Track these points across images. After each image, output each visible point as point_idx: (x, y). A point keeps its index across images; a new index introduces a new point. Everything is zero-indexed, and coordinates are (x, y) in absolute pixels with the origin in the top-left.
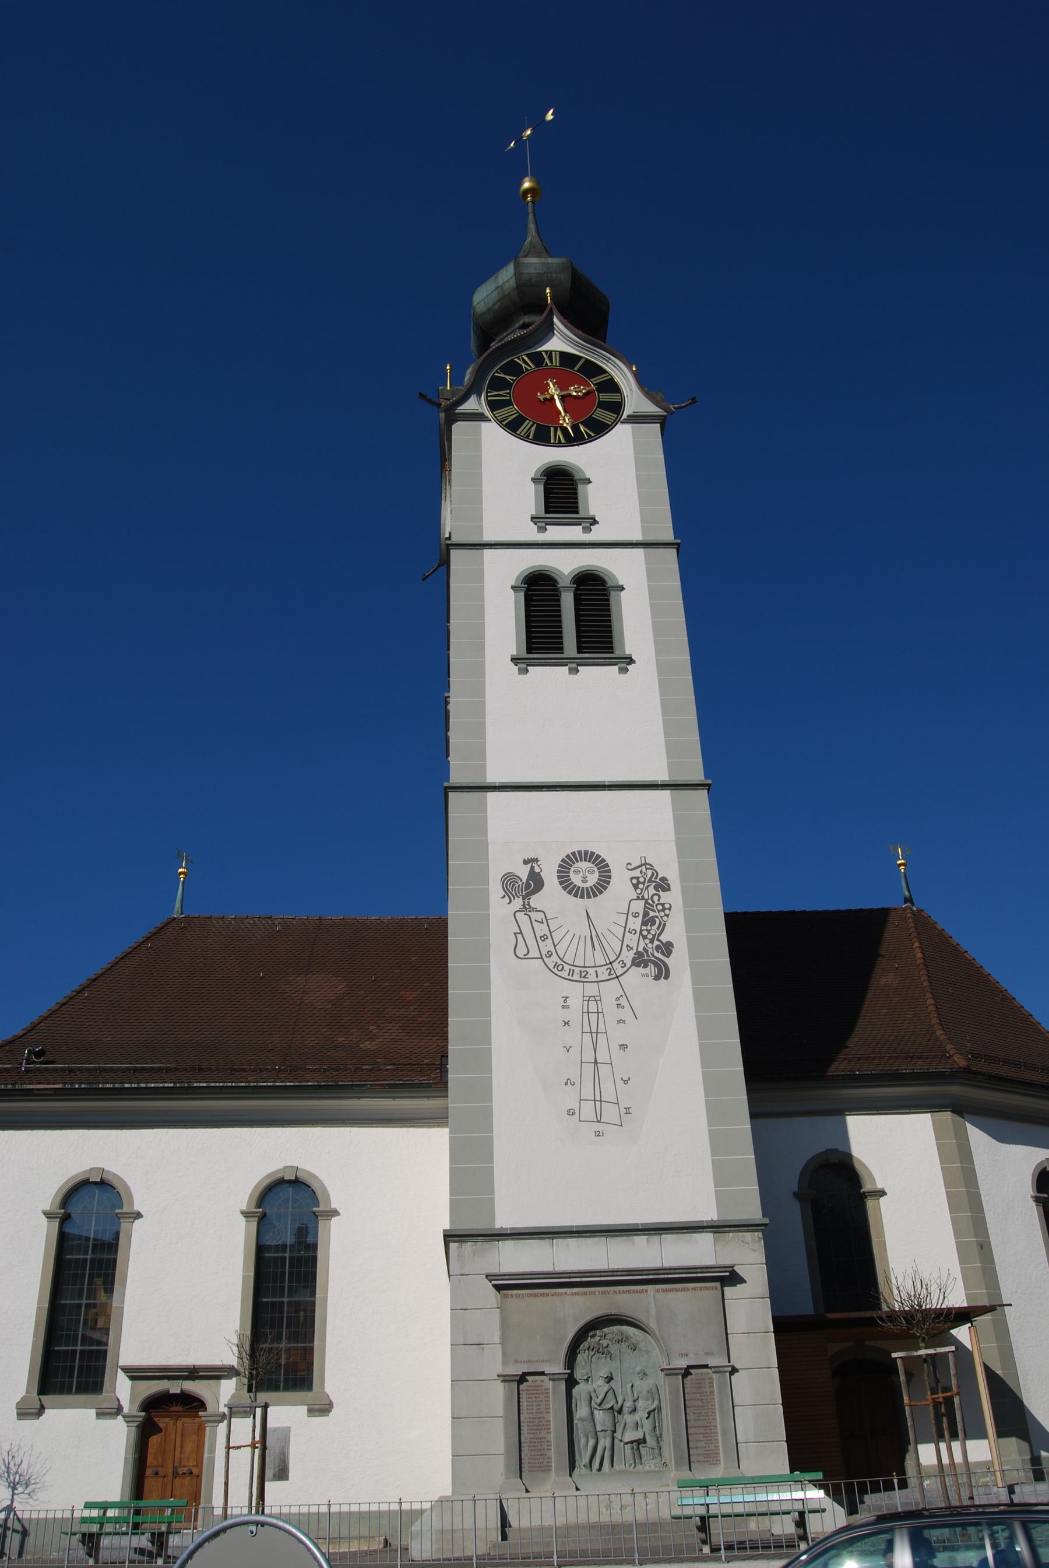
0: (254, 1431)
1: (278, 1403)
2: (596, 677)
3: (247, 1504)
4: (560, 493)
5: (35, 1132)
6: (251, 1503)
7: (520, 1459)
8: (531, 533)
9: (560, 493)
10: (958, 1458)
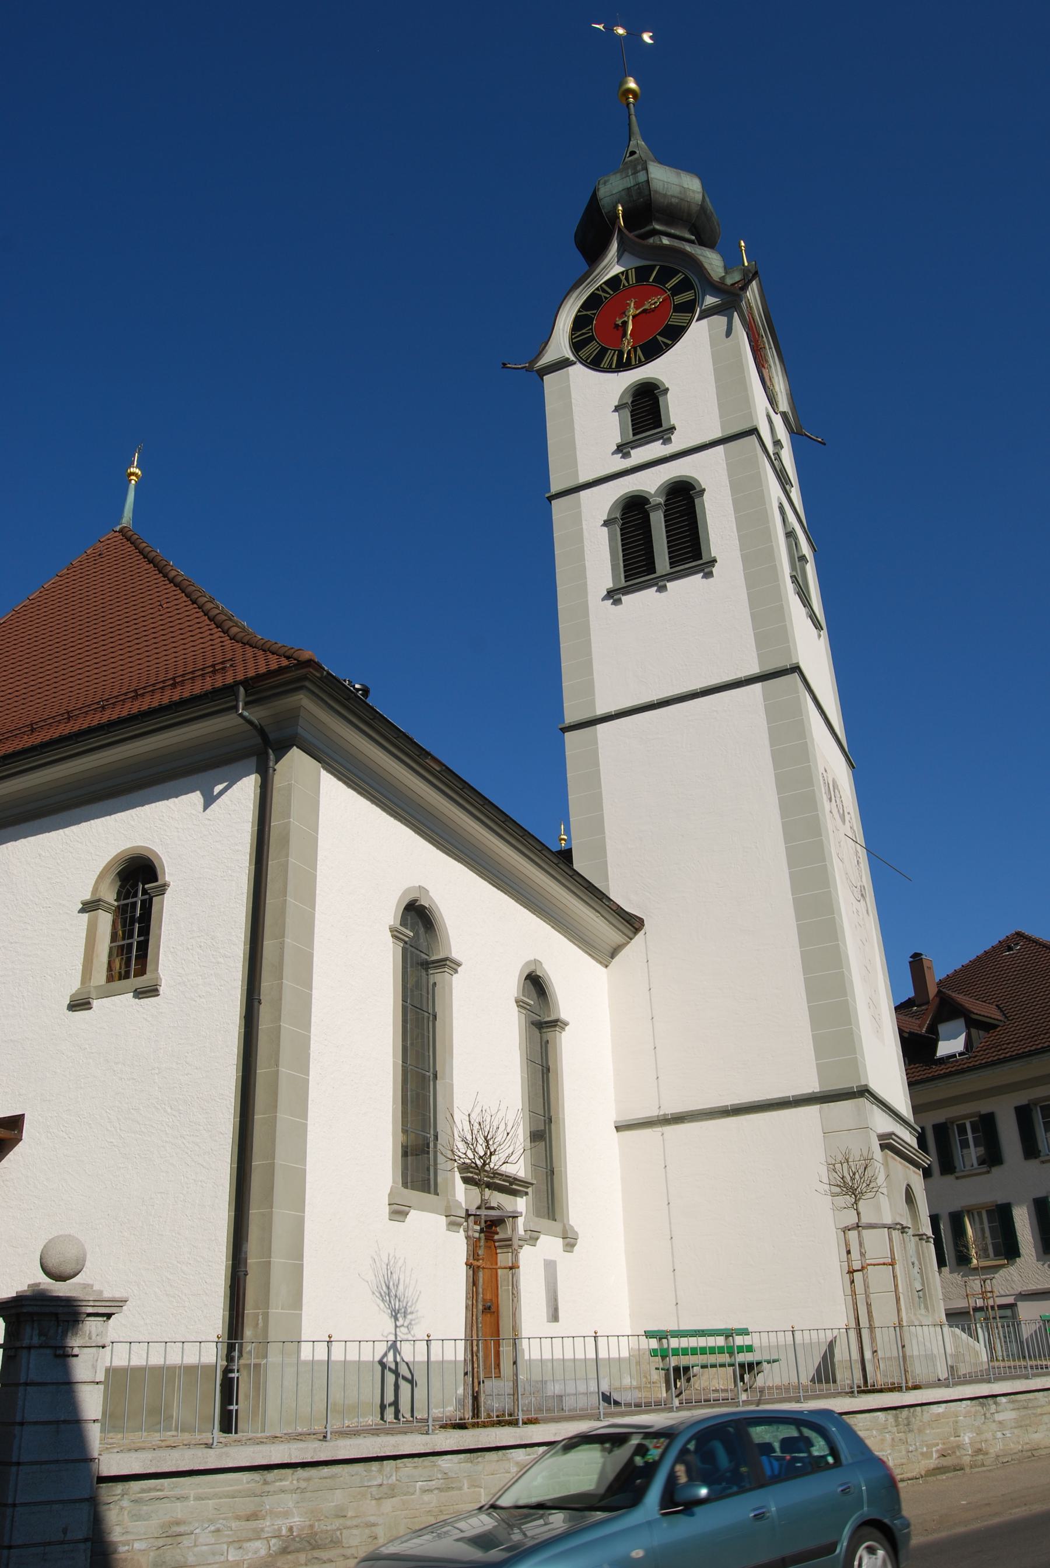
0: (869, 1305)
2: (687, 588)
3: (683, 1327)
4: (646, 412)
5: (374, 806)
8: (620, 463)
9: (646, 412)
10: (666, 1346)
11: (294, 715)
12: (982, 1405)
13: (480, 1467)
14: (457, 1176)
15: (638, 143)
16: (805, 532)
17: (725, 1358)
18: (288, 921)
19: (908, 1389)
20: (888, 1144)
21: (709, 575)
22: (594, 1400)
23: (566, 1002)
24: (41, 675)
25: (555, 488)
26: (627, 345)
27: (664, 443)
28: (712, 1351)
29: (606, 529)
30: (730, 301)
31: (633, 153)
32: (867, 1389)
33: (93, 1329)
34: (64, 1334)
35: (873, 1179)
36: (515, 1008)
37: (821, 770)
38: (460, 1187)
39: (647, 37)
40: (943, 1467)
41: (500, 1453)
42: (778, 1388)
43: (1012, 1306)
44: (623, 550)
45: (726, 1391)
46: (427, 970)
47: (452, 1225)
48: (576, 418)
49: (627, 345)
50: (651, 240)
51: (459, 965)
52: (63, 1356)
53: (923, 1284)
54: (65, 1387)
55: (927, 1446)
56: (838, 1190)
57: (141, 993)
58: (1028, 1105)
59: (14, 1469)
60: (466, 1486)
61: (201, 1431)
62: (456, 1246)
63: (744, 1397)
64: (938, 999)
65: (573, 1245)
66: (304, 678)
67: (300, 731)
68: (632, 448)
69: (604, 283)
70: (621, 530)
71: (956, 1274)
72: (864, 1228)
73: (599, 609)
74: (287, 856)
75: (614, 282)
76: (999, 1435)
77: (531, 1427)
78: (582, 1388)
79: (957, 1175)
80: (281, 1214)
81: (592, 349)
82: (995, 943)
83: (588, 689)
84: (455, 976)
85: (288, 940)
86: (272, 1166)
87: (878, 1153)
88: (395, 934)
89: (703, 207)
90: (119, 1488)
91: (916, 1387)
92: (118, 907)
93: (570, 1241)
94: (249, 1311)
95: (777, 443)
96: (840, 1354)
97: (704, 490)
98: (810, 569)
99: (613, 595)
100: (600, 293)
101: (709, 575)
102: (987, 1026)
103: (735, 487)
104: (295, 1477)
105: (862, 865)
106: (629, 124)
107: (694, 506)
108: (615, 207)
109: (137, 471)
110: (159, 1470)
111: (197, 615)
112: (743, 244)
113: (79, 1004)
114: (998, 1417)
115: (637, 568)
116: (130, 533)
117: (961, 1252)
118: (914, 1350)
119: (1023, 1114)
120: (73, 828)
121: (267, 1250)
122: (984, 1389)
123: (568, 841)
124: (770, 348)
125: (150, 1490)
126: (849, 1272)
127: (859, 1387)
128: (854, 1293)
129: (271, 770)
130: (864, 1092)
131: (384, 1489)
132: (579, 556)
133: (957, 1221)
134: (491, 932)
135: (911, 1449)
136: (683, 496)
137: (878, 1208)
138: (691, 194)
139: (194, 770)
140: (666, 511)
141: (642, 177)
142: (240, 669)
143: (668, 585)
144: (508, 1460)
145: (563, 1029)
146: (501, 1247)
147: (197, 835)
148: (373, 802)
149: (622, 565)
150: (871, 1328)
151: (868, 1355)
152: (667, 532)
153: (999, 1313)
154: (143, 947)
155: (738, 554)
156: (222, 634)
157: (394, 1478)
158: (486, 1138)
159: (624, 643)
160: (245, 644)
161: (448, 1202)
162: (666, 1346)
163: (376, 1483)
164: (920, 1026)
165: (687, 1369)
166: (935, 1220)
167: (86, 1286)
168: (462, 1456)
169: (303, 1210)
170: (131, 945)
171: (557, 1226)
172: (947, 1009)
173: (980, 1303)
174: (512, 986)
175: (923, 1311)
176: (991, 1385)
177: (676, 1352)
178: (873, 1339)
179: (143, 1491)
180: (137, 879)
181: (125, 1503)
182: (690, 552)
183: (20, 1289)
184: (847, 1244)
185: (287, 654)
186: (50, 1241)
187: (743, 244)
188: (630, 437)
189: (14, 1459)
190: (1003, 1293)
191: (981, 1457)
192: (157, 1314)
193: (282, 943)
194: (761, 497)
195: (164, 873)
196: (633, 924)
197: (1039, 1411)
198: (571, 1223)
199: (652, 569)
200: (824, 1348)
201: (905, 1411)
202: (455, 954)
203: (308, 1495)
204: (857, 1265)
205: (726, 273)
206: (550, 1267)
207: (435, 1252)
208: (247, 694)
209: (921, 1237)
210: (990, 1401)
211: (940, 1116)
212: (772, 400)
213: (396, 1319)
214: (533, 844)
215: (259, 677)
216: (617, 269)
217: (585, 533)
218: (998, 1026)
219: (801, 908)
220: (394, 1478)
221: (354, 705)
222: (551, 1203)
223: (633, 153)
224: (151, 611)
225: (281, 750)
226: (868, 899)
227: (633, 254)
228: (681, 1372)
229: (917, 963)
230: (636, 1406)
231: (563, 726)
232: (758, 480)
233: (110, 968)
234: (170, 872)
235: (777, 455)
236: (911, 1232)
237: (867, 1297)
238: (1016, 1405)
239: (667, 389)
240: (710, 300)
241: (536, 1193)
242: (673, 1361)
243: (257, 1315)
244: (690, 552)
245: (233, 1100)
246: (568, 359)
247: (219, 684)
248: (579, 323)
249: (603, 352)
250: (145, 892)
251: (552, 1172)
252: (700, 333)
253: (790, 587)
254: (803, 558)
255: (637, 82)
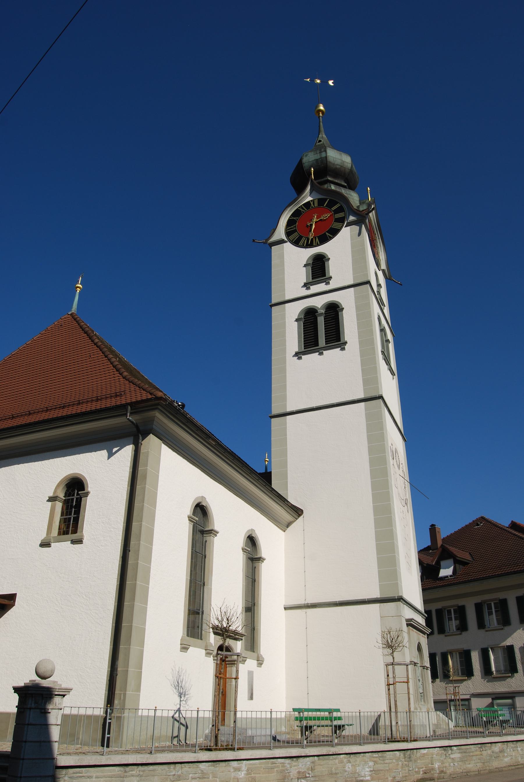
0: (396, 701)
1: (195, 646)
4: (318, 268)
6: (395, 697)
7: (435, 747)
8: (305, 292)
9: (318, 268)
10: (302, 716)
11: (152, 420)
12: (445, 750)
13: (217, 769)
14: (211, 630)
15: (323, 136)
16: (390, 328)
17: (328, 722)
18: (144, 514)
19: (411, 741)
20: (410, 623)
21: (343, 349)
22: (269, 739)
23: (265, 549)
24: (32, 384)
25: (274, 301)
26: (311, 236)
27: (326, 284)
28: (323, 719)
29: (296, 323)
30: (361, 219)
31: (320, 141)
32: (392, 740)
33: (57, 701)
34: (45, 704)
35: (402, 642)
36: (241, 552)
37: (390, 445)
38: (212, 636)
39: (331, 83)
40: (425, 778)
41: (227, 763)
42: (352, 736)
43: (468, 700)
44: (304, 334)
45: (327, 736)
46: (203, 534)
47: (208, 654)
48: (286, 268)
49: (311, 236)
50: (326, 186)
51: (218, 533)
52: (45, 713)
53: (423, 690)
54: (45, 726)
55: (418, 768)
56: (385, 646)
57: (74, 542)
58: (481, 603)
59: (21, 761)
60: (211, 777)
61: (92, 746)
62: (209, 665)
63: (336, 741)
64: (441, 549)
65: (261, 664)
66: (158, 404)
67: (154, 427)
68: (311, 285)
69: (303, 205)
70: (304, 324)
71: (443, 683)
72: (395, 665)
73: (291, 361)
74: (145, 484)
75: (307, 205)
76: (452, 764)
77: (240, 751)
78: (263, 733)
79: (446, 634)
80: (134, 648)
81: (295, 236)
82: (471, 521)
83: (284, 398)
84: (216, 538)
85: (143, 523)
86: (131, 627)
87: (405, 628)
88: (190, 519)
89: (351, 170)
90: (64, 771)
91: (415, 741)
92: (65, 500)
93: (260, 662)
94: (117, 692)
95: (379, 286)
96: (381, 723)
97: (343, 308)
98: (391, 346)
99: (298, 355)
100: (301, 209)
101: (343, 349)
102: (464, 563)
103: (358, 308)
104: (138, 770)
105: (407, 489)
106: (319, 126)
107: (338, 315)
108: (311, 169)
109: (80, 286)
110: (81, 764)
111: (107, 363)
112: (369, 189)
113: (45, 544)
114: (452, 756)
115: (310, 343)
116: (76, 317)
117: (445, 673)
118: (416, 722)
119: (479, 607)
120: (46, 461)
121: (127, 665)
122: (446, 743)
123: (270, 462)
124: (379, 239)
125: (77, 773)
126: (388, 685)
127: (388, 739)
128: (389, 694)
129: (140, 444)
130: (400, 599)
131: (176, 777)
132: (283, 335)
133: (444, 657)
134: (234, 515)
135: (410, 769)
136: (334, 310)
137: (404, 654)
138: (346, 164)
139: (104, 441)
140: (325, 316)
141: (323, 155)
142: (128, 395)
143: (324, 352)
144: (230, 766)
145: (263, 562)
146: (229, 664)
147: (104, 471)
148: (184, 458)
149: (303, 340)
150: (396, 712)
151: (394, 723)
152: (325, 326)
153: (461, 703)
154: (76, 520)
155: (357, 340)
156: (119, 375)
157: (180, 772)
158: (228, 619)
159: (304, 379)
160: (130, 382)
161: (207, 643)
162: (302, 716)
163: (172, 774)
164: (432, 561)
165: (311, 727)
166: (432, 657)
167: (54, 682)
168: (210, 763)
169: (143, 646)
170: (70, 518)
171: (255, 655)
172: (445, 554)
173: (453, 698)
174: (240, 541)
175: (423, 703)
176: (449, 741)
177: (306, 719)
178: (396, 717)
179: (74, 773)
180: (75, 490)
181: (66, 778)
182: (335, 338)
183: (26, 682)
184: (387, 672)
185: (150, 392)
186: (40, 661)
187: (369, 189)
188: (311, 280)
189: (22, 757)
190: (464, 693)
191: (443, 774)
192: (82, 695)
193: (141, 524)
194: (369, 314)
195: (88, 487)
196: (298, 512)
197: (471, 754)
198: (261, 653)
199: (317, 344)
200: (373, 721)
201: (409, 752)
202: (216, 528)
203: (143, 778)
204: (391, 682)
205: (360, 203)
206: (251, 674)
207: (200, 666)
208: (131, 409)
209: (424, 667)
210: (449, 748)
211: (439, 605)
212: (378, 264)
213: (181, 697)
214: (254, 475)
215: (137, 402)
216: (309, 199)
217: (287, 324)
218: (469, 563)
219: (377, 510)
220: (180, 772)
221: (179, 414)
222: (252, 645)
223: (320, 141)
224: (86, 358)
225: (145, 435)
226: (408, 505)
227: (317, 192)
228: (308, 728)
229: (433, 529)
230: (288, 742)
231: (271, 415)
232: (368, 305)
233: (59, 529)
234: (91, 487)
235: (379, 292)
236: (419, 665)
237: (395, 697)
238: (461, 751)
239: (329, 259)
240: (352, 218)
241: (246, 641)
242: (304, 723)
243: (121, 694)
244: (335, 338)
245: (115, 595)
246: (284, 240)
247: (118, 403)
248: (290, 223)
249: (300, 238)
250: (78, 494)
251: (254, 629)
252: (346, 233)
253: (380, 356)
254: (388, 341)
255: (324, 107)
